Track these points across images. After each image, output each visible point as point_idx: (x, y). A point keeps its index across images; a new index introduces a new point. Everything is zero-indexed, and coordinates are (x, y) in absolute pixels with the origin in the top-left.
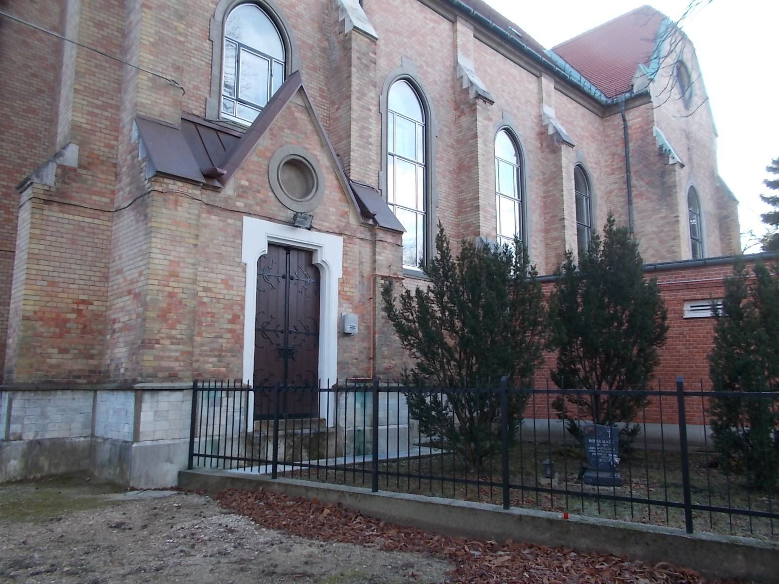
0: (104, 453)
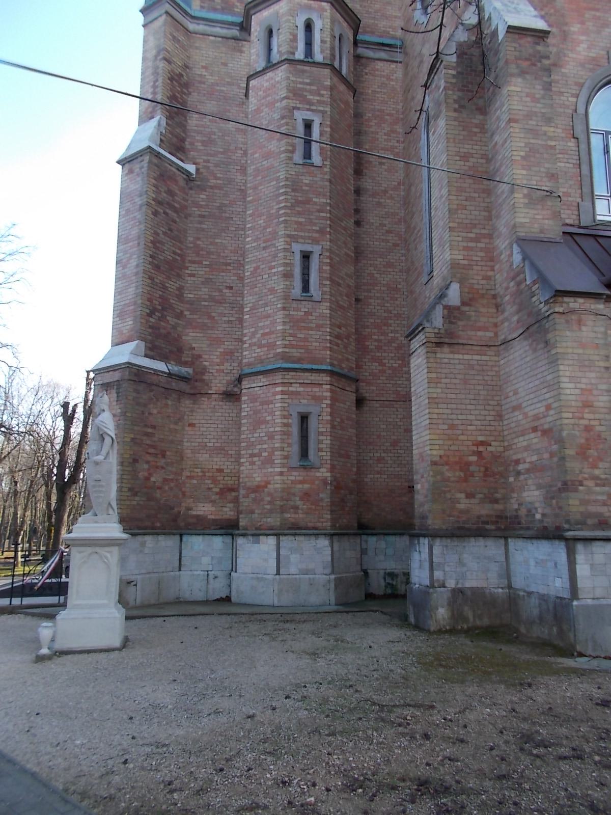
0: (531, 608)
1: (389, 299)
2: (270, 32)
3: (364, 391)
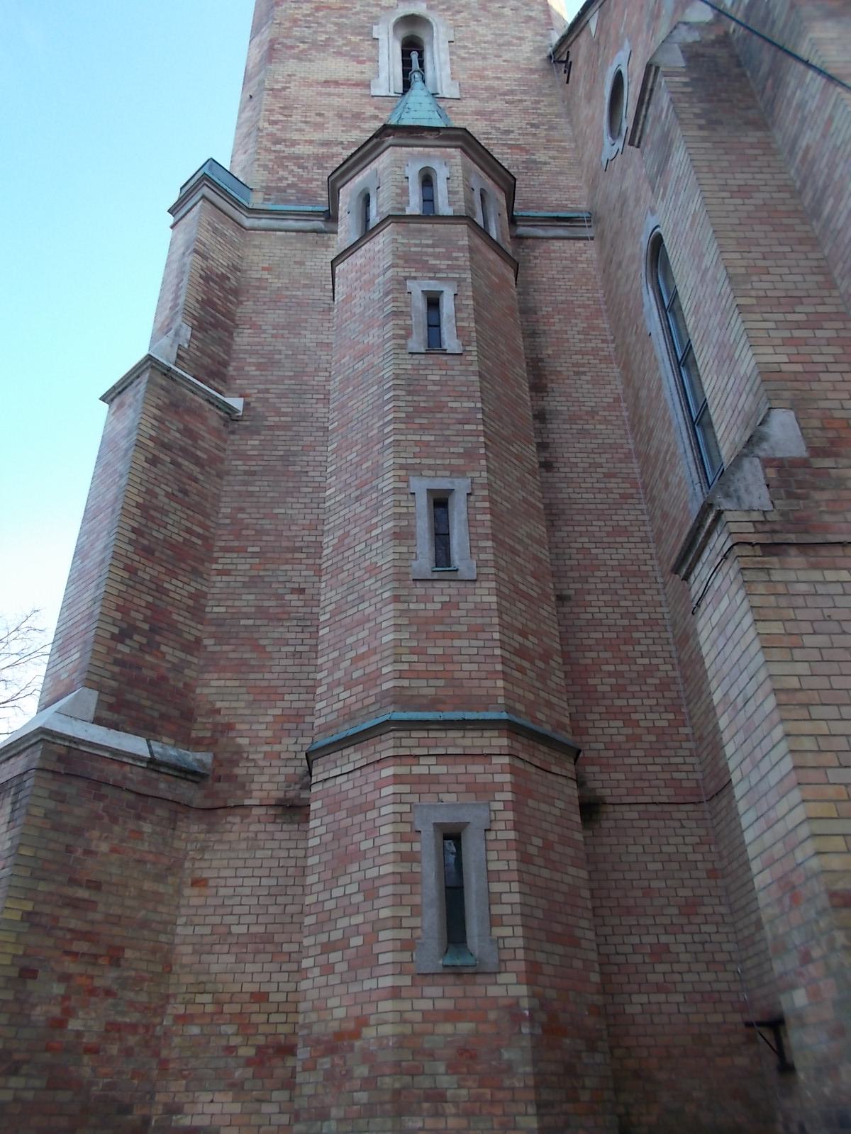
1: (627, 592)
2: (367, 200)
3: (599, 784)
